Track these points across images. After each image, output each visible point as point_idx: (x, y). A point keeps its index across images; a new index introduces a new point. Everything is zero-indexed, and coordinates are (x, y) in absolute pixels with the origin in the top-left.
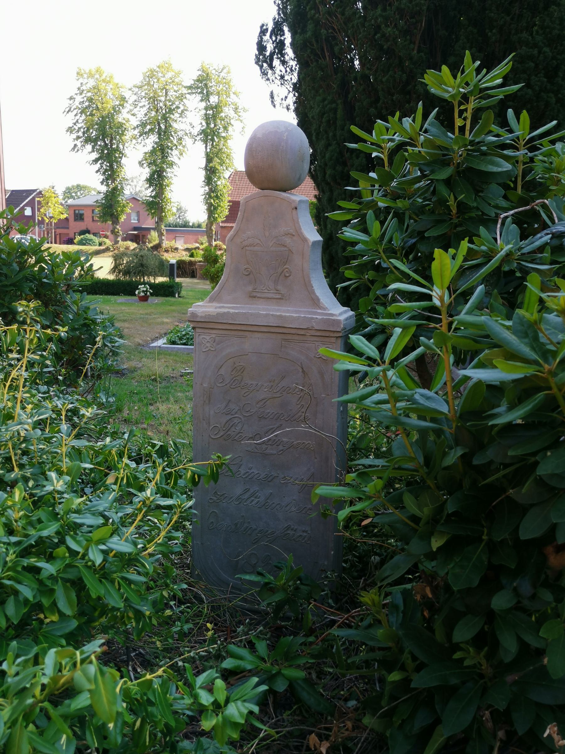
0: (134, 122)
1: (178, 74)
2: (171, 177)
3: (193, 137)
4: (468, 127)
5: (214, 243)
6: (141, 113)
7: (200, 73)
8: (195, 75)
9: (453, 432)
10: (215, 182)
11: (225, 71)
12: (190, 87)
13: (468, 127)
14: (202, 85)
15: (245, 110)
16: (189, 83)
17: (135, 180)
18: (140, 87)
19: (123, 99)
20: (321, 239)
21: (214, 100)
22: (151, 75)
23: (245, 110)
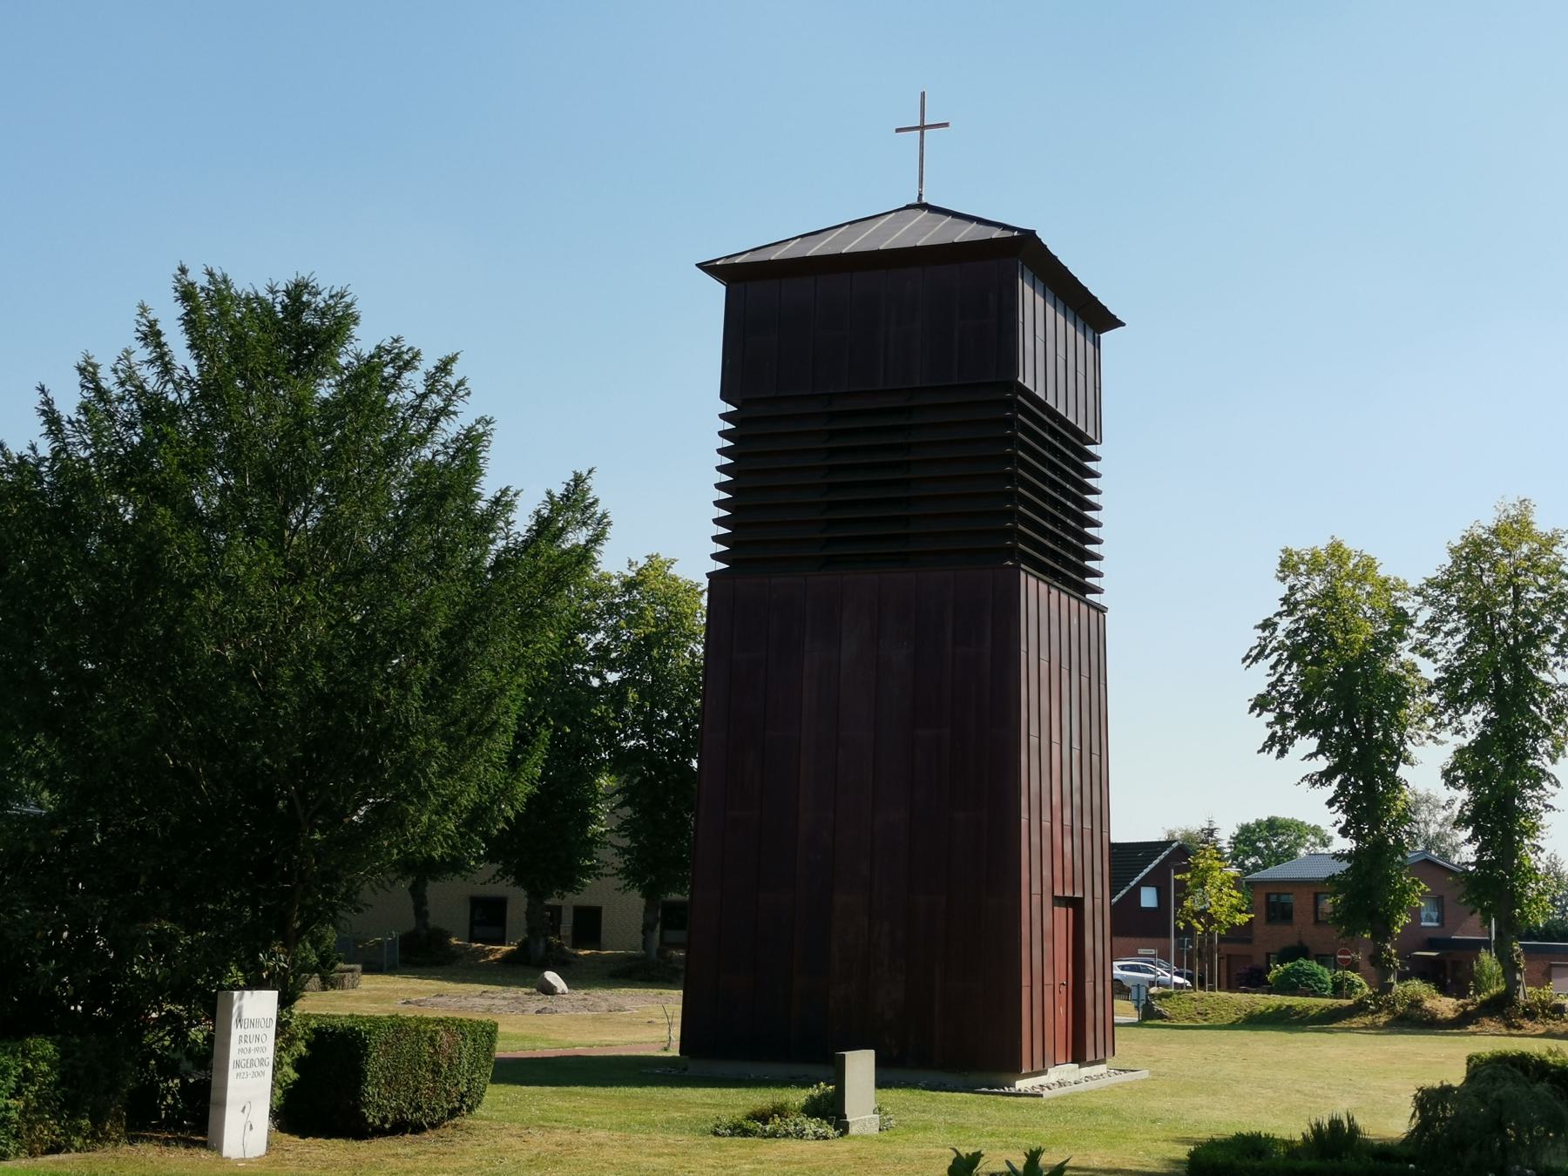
0: (1429, 671)
2: (1536, 812)
6: (1448, 648)
22: (1473, 552)
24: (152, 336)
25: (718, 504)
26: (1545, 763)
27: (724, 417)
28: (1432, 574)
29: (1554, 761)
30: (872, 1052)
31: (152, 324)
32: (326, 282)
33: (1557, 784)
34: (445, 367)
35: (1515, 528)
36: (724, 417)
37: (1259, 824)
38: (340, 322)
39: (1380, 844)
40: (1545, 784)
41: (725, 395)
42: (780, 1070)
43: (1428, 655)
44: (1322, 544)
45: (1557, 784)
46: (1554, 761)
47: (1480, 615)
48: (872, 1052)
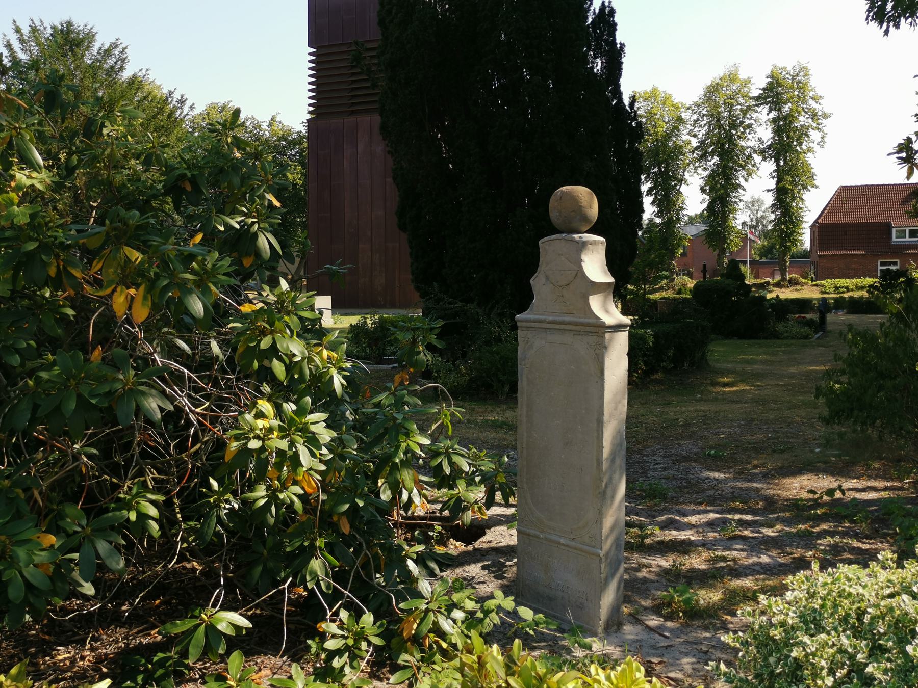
0: (695, 143)
1: (747, 82)
2: (736, 202)
3: (762, 152)
4: (178, 247)
5: (788, 277)
6: (701, 132)
7: (770, 80)
8: (763, 82)
9: (402, 438)
10: (788, 203)
11: (802, 74)
12: (757, 98)
13: (178, 247)
14: (773, 93)
15: (826, 116)
16: (755, 93)
17: (756, 205)
18: (698, 105)
19: (680, 120)
20: (612, 280)
21: (786, 108)
22: (713, 90)
23: (826, 116)
24: (9, 46)
25: (310, 90)
26: (741, 181)
27: (310, 54)
28: (696, 99)
29: (746, 180)
30: (330, 297)
31: (8, 42)
32: (80, 22)
33: (744, 190)
34: (124, 49)
35: (732, 78)
36: (310, 54)
37: (696, 215)
38: (90, 37)
39: (670, 219)
40: (740, 190)
41: (310, 45)
42: (353, 311)
43: (695, 136)
44: (649, 89)
45: (744, 190)
46: (746, 180)
47: (715, 117)
48: (330, 297)
